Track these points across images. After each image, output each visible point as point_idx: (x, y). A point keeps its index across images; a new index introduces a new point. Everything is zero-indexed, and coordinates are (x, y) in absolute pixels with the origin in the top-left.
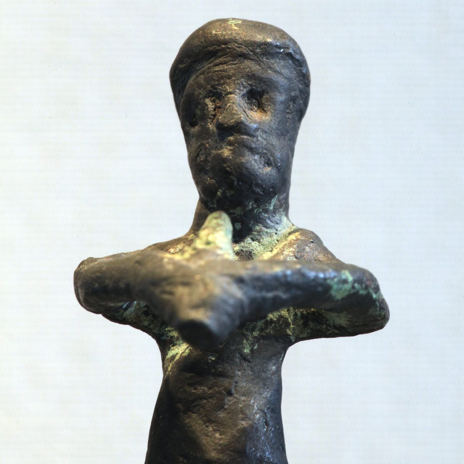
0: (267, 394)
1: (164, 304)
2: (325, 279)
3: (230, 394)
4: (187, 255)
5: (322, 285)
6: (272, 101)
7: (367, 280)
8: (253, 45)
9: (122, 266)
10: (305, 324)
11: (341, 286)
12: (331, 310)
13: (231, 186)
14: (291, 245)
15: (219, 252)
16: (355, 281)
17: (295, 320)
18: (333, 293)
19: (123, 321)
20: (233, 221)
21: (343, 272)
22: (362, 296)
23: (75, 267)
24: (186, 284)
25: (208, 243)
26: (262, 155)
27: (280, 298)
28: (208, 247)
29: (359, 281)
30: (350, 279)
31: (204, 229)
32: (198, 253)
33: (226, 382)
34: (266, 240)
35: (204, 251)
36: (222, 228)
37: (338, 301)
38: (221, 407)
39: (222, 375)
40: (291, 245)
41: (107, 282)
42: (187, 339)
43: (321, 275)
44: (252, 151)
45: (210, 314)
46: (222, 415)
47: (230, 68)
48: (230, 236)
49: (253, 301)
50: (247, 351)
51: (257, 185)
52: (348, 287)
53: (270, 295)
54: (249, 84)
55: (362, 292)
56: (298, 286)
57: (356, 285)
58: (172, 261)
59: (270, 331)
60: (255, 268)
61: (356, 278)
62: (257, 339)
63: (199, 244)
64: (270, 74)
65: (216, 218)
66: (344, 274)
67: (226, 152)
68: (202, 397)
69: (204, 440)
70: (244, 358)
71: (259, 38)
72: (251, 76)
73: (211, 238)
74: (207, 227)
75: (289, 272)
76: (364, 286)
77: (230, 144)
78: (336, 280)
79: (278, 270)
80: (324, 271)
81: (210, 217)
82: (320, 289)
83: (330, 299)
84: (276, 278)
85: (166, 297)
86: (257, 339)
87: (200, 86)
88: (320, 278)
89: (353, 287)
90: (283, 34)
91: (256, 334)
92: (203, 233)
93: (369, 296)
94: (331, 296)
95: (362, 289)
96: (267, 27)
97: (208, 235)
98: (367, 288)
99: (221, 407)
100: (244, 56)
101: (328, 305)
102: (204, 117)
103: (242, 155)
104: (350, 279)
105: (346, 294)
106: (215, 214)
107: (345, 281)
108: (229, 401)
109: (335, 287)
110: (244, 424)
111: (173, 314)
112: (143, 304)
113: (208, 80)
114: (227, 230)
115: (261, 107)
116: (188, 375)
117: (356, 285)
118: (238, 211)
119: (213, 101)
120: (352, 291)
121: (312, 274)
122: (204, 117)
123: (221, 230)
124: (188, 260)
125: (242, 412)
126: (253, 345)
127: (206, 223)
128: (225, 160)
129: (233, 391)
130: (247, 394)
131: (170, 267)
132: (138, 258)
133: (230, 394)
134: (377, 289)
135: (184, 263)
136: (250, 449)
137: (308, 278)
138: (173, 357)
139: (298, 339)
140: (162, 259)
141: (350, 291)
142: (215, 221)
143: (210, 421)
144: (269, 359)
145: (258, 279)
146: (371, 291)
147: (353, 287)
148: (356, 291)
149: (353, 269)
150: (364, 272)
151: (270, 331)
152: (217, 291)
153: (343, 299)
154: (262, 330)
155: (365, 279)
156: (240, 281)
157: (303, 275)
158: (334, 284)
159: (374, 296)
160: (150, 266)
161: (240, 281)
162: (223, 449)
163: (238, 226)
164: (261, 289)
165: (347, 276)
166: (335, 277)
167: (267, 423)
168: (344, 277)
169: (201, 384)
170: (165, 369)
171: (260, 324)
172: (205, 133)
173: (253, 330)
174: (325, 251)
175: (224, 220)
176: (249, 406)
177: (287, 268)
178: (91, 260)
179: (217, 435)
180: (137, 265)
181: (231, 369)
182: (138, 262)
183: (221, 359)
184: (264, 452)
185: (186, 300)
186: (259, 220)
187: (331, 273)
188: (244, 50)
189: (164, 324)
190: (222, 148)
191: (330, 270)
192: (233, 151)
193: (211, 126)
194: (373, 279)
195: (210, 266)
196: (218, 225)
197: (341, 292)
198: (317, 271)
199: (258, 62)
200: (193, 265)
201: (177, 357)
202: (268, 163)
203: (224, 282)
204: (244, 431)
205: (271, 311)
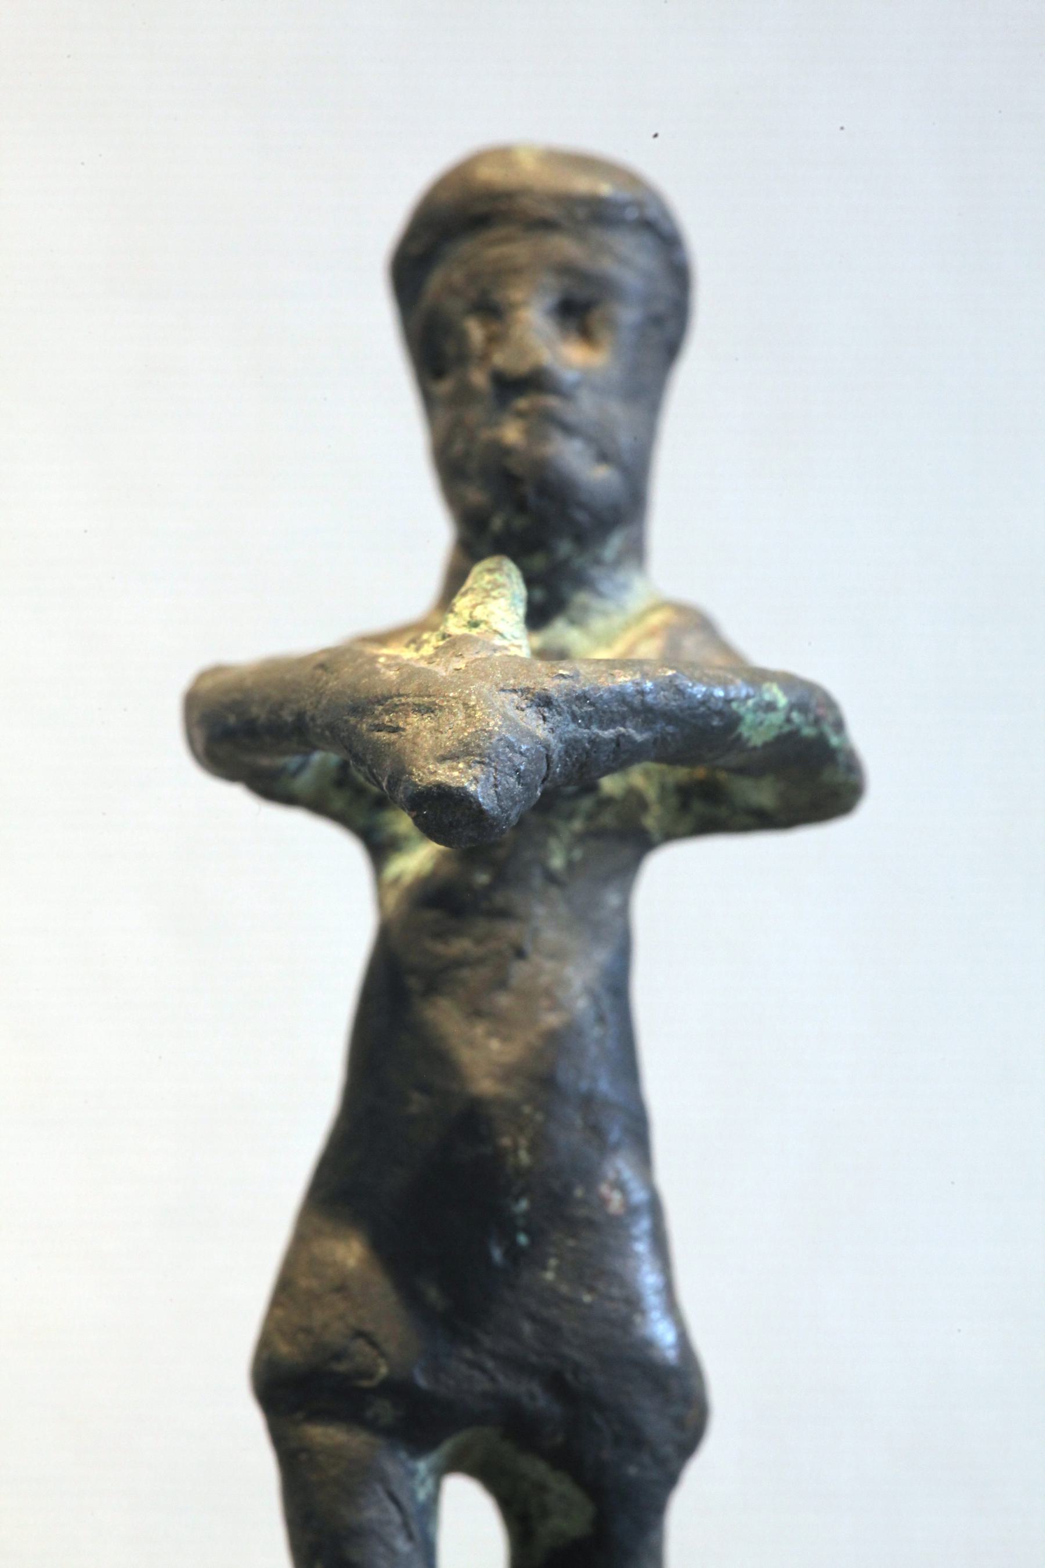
0: (602, 955)
1: (378, 751)
2: (728, 701)
3: (520, 954)
5: (720, 713)
6: (611, 324)
7: (818, 705)
8: (569, 201)
9: (288, 677)
10: (684, 806)
11: (761, 715)
12: (741, 771)
13: (521, 506)
14: (652, 634)
15: (497, 641)
16: (792, 707)
18: (744, 730)
19: (288, 799)
20: (530, 581)
21: (766, 686)
23: (181, 682)
24: (428, 709)
25: (474, 624)
26: (589, 440)
27: (629, 739)
28: (474, 632)
29: (801, 706)
30: (782, 701)
31: (465, 594)
32: (452, 645)
33: (512, 931)
34: (598, 624)
35: (465, 638)
37: (755, 748)
38: (502, 984)
39: (504, 914)
40: (652, 634)
41: (255, 710)
42: (430, 830)
43: (719, 693)
44: (569, 430)
46: (503, 1000)
48: (521, 610)
49: (571, 745)
51: (582, 506)
52: (776, 718)
53: (608, 734)
54: (602, 687)
55: (808, 731)
56: (668, 716)
57: (795, 716)
58: (395, 663)
59: (607, 819)
60: (575, 676)
61: (794, 700)
62: (580, 838)
63: (454, 625)
64: (607, 266)
65: (490, 571)
66: (769, 690)
67: (512, 433)
68: (460, 963)
69: (465, 1055)
70: (551, 878)
71: (582, 184)
72: (566, 270)
73: (479, 613)
74: (472, 589)
75: (649, 685)
76: (811, 717)
77: (521, 415)
78: (750, 703)
79: (624, 680)
80: (725, 684)
81: (477, 569)
82: (716, 722)
83: (739, 743)
84: (621, 696)
85: (384, 736)
86: (580, 838)
88: (718, 699)
89: (788, 720)
91: (577, 825)
92: (462, 603)
94: (739, 737)
95: (808, 724)
97: (474, 606)
98: (817, 722)
99: (502, 984)
100: (546, 225)
101: (734, 759)
102: (463, 358)
104: (782, 701)
105: (773, 734)
106: (489, 563)
108: (519, 971)
109: (749, 718)
110: (552, 1020)
111: (399, 774)
114: (514, 596)
115: (586, 335)
117: (795, 716)
118: (538, 562)
120: (787, 729)
121: (699, 691)
122: (463, 358)
123: (503, 596)
124: (430, 660)
125: (548, 993)
126: (569, 849)
127: (469, 583)
128: (504, 451)
129: (528, 947)
130: (558, 955)
132: (322, 658)
133: (520, 954)
134: (839, 726)
135: (423, 664)
136: (565, 1075)
137: (692, 696)
138: (397, 880)
139: (670, 836)
140: (374, 659)
141: (781, 727)
142: (487, 577)
145: (583, 698)
146: (828, 730)
147: (788, 720)
149: (788, 682)
150: (812, 688)
151: (607, 819)
152: (495, 724)
153: (766, 745)
154: (590, 817)
156: (544, 702)
157: (680, 692)
158: (745, 710)
159: (834, 741)
161: (544, 702)
162: (508, 1074)
163: (539, 595)
164: (588, 720)
167: (601, 1019)
168: (767, 697)
170: (381, 903)
171: (586, 804)
172: (464, 395)
173: (570, 816)
174: (725, 648)
175: (509, 576)
177: (645, 675)
178: (218, 670)
179: (495, 1044)
180: (319, 672)
181: (529, 776)
182: (322, 666)
183: (501, 878)
185: (427, 741)
186: (582, 581)
187: (740, 689)
188: (550, 211)
189: (381, 803)
191: (739, 682)
192: (528, 432)
193: (479, 378)
194: (830, 704)
195: (478, 668)
196: (497, 585)
197: (761, 729)
198: (708, 685)
200: (441, 670)
202: (603, 457)
204: (554, 1039)
205: (609, 771)
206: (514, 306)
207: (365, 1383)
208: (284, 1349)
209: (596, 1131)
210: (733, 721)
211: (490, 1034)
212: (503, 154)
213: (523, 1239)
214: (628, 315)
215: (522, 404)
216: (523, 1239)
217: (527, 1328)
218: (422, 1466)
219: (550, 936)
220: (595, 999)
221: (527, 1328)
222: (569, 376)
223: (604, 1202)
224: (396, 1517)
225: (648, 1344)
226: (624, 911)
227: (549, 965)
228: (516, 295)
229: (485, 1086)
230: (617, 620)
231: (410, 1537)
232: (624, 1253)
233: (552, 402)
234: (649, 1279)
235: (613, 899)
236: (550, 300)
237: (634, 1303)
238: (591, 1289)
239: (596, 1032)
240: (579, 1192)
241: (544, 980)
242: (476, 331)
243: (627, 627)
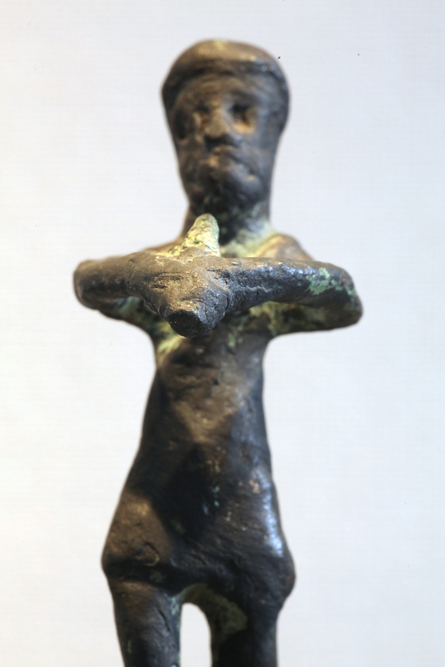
0: (251, 384)
1: (156, 296)
2: (304, 275)
3: (216, 383)
4: (177, 253)
5: (301, 280)
6: (255, 115)
7: (343, 277)
8: (237, 63)
9: (118, 265)
10: (286, 320)
11: (319, 282)
12: (311, 305)
13: (217, 193)
14: (272, 247)
15: (207, 250)
16: (332, 278)
17: (277, 316)
18: (311, 288)
20: (221, 224)
21: (321, 269)
22: (337, 292)
24: (177, 279)
25: (197, 243)
26: (246, 165)
27: (263, 291)
28: (197, 246)
29: (335, 278)
30: (328, 275)
31: (193, 230)
32: (187, 251)
33: (213, 373)
34: (249, 243)
35: (193, 248)
36: (209, 228)
37: (316, 296)
38: (208, 395)
39: (209, 366)
40: (272, 247)
41: (104, 279)
42: (178, 330)
43: (301, 272)
44: (237, 160)
45: (198, 304)
46: (209, 402)
47: (216, 84)
48: (217, 237)
49: (238, 294)
50: (232, 344)
52: (325, 283)
53: (254, 289)
55: (339, 288)
56: (279, 282)
57: (333, 281)
59: (253, 326)
60: (240, 265)
61: (332, 275)
62: (241, 334)
63: (188, 243)
64: (254, 91)
65: (204, 220)
66: (322, 271)
67: (213, 162)
68: (190, 386)
69: (193, 426)
70: (229, 350)
71: (243, 56)
72: (236, 92)
73: (199, 238)
75: (271, 268)
76: (340, 282)
77: (217, 154)
79: (261, 266)
80: (303, 268)
81: (198, 219)
84: (259, 273)
86: (241, 334)
87: (188, 101)
89: (330, 284)
90: (264, 54)
91: (240, 328)
92: (191, 234)
93: (344, 292)
94: (309, 290)
95: (338, 285)
96: (196, 268)
97: (197, 235)
98: (342, 284)
99: (208, 395)
100: (228, 73)
101: (306, 300)
102: (192, 130)
103: (227, 164)
104: (328, 275)
105: (324, 289)
106: (203, 217)
107: (323, 278)
108: (216, 390)
109: (313, 282)
110: (229, 411)
111: (165, 305)
112: (137, 299)
113: (196, 96)
114: (214, 231)
115: (245, 120)
116: (178, 366)
117: (333, 281)
118: (224, 217)
119: (201, 115)
120: (329, 287)
121: (292, 271)
123: (209, 231)
124: (178, 258)
125: (228, 399)
126: (237, 338)
127: (195, 225)
128: (210, 169)
129: (219, 380)
130: (232, 383)
131: (162, 264)
132: (132, 257)
133: (216, 383)
134: (352, 286)
135: (175, 259)
136: (235, 434)
137: (289, 273)
138: (164, 351)
139: (280, 333)
140: (154, 257)
141: (327, 287)
142: (202, 223)
143: (197, 408)
144: (252, 352)
145: (243, 274)
146: (347, 288)
147: (330, 284)
148: (332, 287)
149: (330, 267)
150: (340, 270)
151: (253, 326)
152: (205, 285)
153: (320, 294)
155: (341, 276)
156: (226, 275)
157: (284, 271)
159: (350, 293)
160: (143, 263)
161: (226, 275)
162: (210, 433)
163: (224, 230)
164: (245, 283)
165: (325, 274)
166: (313, 274)
167: (250, 410)
168: (321, 274)
169: (190, 374)
170: (157, 361)
171: (244, 319)
172: (193, 145)
173: (237, 325)
174: (304, 254)
175: (211, 222)
176: (234, 395)
177: (269, 264)
178: (88, 262)
179: (205, 421)
180: (131, 263)
182: (132, 260)
183: (208, 351)
184: (247, 436)
185: (177, 292)
186: (243, 225)
187: (310, 270)
188: (229, 67)
189: (157, 319)
190: (207, 158)
191: (309, 267)
192: (220, 162)
193: (199, 138)
194: (348, 277)
195: (199, 262)
196: (207, 226)
199: (243, 78)
200: (183, 262)
201: (168, 351)
202: (252, 172)
203: (211, 275)
206: (214, 108)
207: (150, 565)
208: (115, 550)
209: (248, 458)
210: (307, 284)
211: (203, 417)
212: (209, 43)
213: (217, 504)
214: (263, 112)
215: (218, 149)
216: (217, 504)
217: (219, 541)
218: (174, 600)
219: (229, 375)
220: (248, 403)
221: (219, 541)
222: (237, 138)
223: (251, 488)
224: (163, 621)
225: (270, 548)
226: (260, 364)
227: (228, 387)
228: (215, 103)
229: (201, 439)
230: (258, 241)
231: (169, 630)
232: (260, 510)
233: (230, 148)
234: (270, 521)
235: (256, 360)
236: (229, 105)
237: (264, 531)
238: (246, 525)
239: (248, 416)
240: (241, 484)
241: (226, 394)
242: (198, 118)
243: (262, 244)
